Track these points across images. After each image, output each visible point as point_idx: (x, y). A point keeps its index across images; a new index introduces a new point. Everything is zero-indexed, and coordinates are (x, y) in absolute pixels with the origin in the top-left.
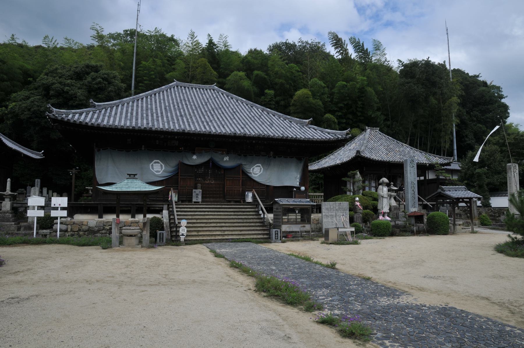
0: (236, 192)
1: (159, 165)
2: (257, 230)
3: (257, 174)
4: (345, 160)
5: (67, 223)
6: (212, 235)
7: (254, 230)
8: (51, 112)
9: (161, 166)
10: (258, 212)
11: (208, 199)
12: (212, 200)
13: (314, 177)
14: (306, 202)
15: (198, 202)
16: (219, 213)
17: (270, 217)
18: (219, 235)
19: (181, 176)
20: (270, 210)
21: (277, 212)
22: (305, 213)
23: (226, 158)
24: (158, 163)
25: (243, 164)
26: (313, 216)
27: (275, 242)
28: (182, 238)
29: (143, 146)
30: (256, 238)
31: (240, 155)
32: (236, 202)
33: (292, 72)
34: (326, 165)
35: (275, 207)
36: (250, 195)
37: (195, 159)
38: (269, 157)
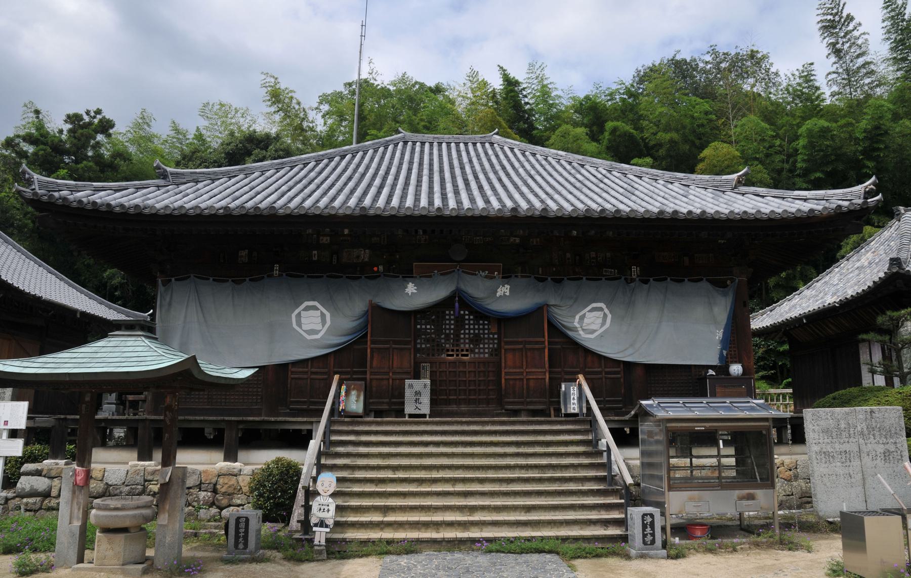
0: (532, 383)
1: (318, 313)
2: (583, 507)
3: (593, 331)
4: (851, 292)
5: (53, 474)
6: (426, 525)
7: (572, 507)
8: (29, 182)
9: (323, 316)
10: (594, 443)
11: (454, 408)
12: (464, 408)
13: (761, 351)
14: (752, 409)
15: (424, 416)
16: (469, 450)
17: (624, 462)
18: (451, 524)
19: (373, 342)
20: (624, 439)
21: (650, 444)
22: (753, 448)
23: (504, 290)
24: (315, 308)
25: (552, 302)
26: (783, 457)
27: (642, 556)
28: (320, 535)
29: (277, 267)
30: (576, 539)
31: (542, 280)
32: (534, 413)
33: (693, 117)
34: (795, 313)
35: (644, 427)
36: (574, 391)
37: (413, 295)
38: (629, 281)
